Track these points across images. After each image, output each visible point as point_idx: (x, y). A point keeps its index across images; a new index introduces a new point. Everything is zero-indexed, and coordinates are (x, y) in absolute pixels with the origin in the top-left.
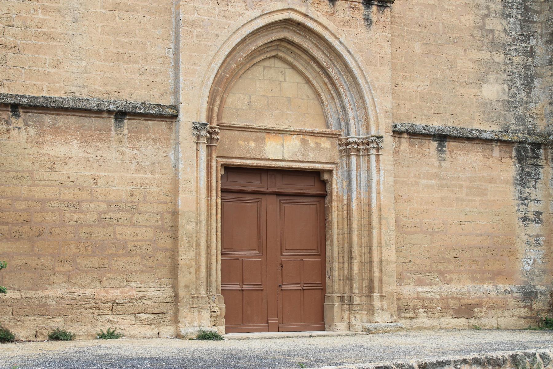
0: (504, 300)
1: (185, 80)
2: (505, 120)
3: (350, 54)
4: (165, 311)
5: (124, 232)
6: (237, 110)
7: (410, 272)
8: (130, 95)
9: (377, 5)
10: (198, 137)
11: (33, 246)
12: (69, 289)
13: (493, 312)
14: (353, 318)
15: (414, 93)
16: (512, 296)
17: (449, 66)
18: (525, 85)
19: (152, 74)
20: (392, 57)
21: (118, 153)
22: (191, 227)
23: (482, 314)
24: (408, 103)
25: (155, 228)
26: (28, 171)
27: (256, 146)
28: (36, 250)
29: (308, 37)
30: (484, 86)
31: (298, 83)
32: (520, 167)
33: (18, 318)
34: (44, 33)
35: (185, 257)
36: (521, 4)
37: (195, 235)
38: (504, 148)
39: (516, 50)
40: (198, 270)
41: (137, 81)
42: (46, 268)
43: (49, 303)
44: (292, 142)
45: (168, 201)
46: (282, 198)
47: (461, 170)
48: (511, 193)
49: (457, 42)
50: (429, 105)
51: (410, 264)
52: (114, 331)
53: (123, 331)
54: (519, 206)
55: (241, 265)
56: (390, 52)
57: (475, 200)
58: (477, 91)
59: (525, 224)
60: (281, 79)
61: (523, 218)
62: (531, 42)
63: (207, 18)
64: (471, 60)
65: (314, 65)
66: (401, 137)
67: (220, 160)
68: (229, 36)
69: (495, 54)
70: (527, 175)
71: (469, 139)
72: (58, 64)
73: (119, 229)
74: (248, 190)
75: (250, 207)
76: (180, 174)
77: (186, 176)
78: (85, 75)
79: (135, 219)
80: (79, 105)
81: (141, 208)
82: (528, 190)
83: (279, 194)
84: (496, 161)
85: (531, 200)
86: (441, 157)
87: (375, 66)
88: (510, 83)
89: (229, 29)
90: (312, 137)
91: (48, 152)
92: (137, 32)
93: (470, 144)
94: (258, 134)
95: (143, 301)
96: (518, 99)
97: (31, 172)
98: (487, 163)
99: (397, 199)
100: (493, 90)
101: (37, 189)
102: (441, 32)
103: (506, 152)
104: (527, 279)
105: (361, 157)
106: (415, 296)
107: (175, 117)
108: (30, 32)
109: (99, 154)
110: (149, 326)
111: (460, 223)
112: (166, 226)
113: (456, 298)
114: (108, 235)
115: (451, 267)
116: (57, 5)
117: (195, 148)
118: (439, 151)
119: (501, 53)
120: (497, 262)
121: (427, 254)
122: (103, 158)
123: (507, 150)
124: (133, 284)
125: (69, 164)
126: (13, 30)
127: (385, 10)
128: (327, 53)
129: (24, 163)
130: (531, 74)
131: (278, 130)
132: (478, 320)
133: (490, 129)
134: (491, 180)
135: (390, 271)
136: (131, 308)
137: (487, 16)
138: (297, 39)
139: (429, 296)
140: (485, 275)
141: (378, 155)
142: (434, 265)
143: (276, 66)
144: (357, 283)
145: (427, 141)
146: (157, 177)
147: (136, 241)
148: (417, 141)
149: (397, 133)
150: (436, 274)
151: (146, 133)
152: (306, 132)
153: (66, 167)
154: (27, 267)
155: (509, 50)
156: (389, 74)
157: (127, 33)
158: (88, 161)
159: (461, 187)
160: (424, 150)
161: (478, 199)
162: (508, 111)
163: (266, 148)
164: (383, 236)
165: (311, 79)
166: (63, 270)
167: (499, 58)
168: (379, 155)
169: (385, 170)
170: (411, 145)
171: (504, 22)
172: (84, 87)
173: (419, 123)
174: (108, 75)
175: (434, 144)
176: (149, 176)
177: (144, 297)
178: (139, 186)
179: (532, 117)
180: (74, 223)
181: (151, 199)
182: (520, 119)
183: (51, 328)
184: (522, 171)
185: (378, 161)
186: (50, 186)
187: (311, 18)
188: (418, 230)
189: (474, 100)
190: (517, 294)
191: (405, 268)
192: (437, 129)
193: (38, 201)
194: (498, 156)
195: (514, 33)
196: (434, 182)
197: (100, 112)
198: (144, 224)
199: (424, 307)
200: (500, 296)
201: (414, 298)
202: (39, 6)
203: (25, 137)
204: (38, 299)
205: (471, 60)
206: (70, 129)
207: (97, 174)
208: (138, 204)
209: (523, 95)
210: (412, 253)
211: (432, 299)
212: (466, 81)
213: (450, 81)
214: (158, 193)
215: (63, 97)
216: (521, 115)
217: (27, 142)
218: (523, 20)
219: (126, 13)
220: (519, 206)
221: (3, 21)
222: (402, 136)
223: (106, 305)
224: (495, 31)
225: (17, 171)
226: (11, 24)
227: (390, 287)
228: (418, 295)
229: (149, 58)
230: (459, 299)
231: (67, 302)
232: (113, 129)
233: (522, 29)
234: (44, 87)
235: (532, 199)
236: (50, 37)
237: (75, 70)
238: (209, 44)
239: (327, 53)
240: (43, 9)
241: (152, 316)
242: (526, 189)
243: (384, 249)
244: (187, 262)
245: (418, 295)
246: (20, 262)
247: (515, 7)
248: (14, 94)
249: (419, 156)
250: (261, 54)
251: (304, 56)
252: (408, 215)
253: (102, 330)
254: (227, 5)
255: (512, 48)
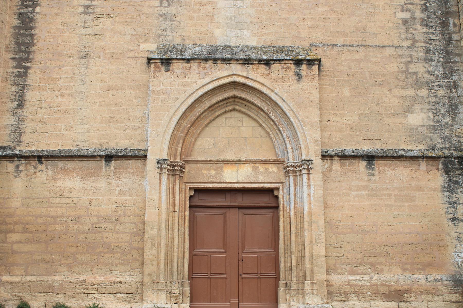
0: (433, 287)
1: (152, 131)
2: (431, 140)
3: (284, 101)
4: (136, 292)
5: (109, 237)
6: (205, 149)
7: (343, 264)
8: (117, 144)
9: (306, 64)
10: (161, 169)
11: (47, 247)
12: (70, 275)
13: (423, 297)
14: (292, 301)
15: (344, 126)
16: (442, 283)
17: (376, 103)
18: (449, 112)
19: (133, 129)
20: (320, 101)
21: (107, 183)
22: (154, 232)
23: (412, 299)
24: (339, 134)
25: (132, 233)
26: (47, 198)
27: (216, 174)
28: (50, 249)
29: (252, 93)
30: (410, 115)
31: (253, 127)
32: (448, 177)
33: (33, 294)
34: (61, 110)
35: (150, 253)
36: (443, 50)
37: (156, 238)
38: (431, 163)
39: (439, 85)
40: (158, 263)
41: (122, 135)
42: (55, 261)
43: (54, 285)
44: (245, 169)
45: (141, 215)
46: (244, 210)
47: (390, 182)
48: (439, 200)
49: (383, 84)
50: (358, 133)
51: (343, 257)
52: (98, 305)
53: (105, 305)
54: (447, 208)
55: (209, 259)
56: (318, 96)
57: (404, 206)
58: (402, 120)
59: (454, 224)
60: (240, 125)
61: (453, 218)
62: (453, 78)
63: (170, 87)
64: (397, 97)
65: (262, 113)
66: (333, 160)
67: (187, 185)
68: (185, 98)
69: (419, 90)
70: (455, 183)
71: (394, 157)
72: (69, 128)
73: (105, 235)
74: (260, 206)
75: (217, 218)
76: (147, 195)
77: (151, 196)
78: (87, 134)
79: (117, 227)
80: (80, 153)
81: (122, 220)
82: (457, 196)
83: (240, 208)
84: (423, 173)
85: (460, 204)
86: (370, 173)
87: (305, 108)
88: (435, 112)
89: (186, 93)
90: (262, 164)
91: (60, 185)
92: (123, 103)
93: (397, 162)
94: (218, 165)
95: (120, 284)
96: (443, 123)
97: (49, 198)
98: (415, 175)
99: (326, 206)
100: (418, 118)
101: (52, 209)
102: (368, 78)
103: (432, 165)
104: (458, 269)
105: (298, 176)
106: (346, 283)
107: (146, 156)
108: (52, 110)
109: (93, 184)
110: (123, 303)
111: (390, 224)
112: (139, 232)
113: (386, 285)
114: (98, 239)
115: (382, 260)
116: (71, 92)
117: (158, 177)
118: (368, 168)
119: (425, 89)
120: (427, 255)
121: (358, 249)
122: (96, 187)
123: (434, 164)
124: (115, 273)
125: (73, 192)
126: (42, 110)
127: (314, 67)
128: (268, 103)
129: (44, 193)
130: (455, 103)
131: (233, 161)
132: (408, 303)
133: (417, 149)
134: (419, 189)
135: (320, 263)
136: (111, 289)
137: (409, 62)
138: (243, 95)
139: (359, 283)
140: (415, 267)
141: (309, 174)
142: (365, 259)
143: (235, 116)
144: (295, 273)
145: (357, 162)
146: (134, 198)
147: (117, 243)
148: (347, 162)
149: (324, 156)
150: (368, 266)
151: (126, 169)
152: (255, 161)
153: (71, 194)
154: (43, 260)
155: (433, 86)
156: (318, 113)
157: (116, 104)
158: (86, 189)
159: (390, 195)
160: (355, 168)
161: (406, 204)
162: (434, 133)
163: (224, 174)
164: (314, 236)
165: (261, 123)
166: (66, 262)
167: (424, 93)
168: (310, 174)
169: (315, 185)
170: (342, 165)
171: (426, 65)
172: (85, 142)
173: (349, 149)
174: (102, 133)
175: (363, 164)
176: (128, 198)
177: (120, 282)
178: (121, 205)
179: (459, 137)
180: (75, 231)
181: (129, 213)
182: (444, 139)
183: (55, 301)
184: (450, 180)
185: (309, 179)
186: (60, 207)
187: (252, 79)
188: (349, 230)
189: (401, 127)
190: (447, 282)
191: (339, 261)
192: (365, 152)
193: (51, 217)
194: (425, 169)
195: (436, 72)
196: (364, 192)
197: (93, 157)
198: (123, 231)
199: (354, 292)
200: (430, 284)
201: (345, 285)
202: (59, 94)
203: (46, 176)
204: (47, 282)
205: (397, 97)
206: (75, 169)
207: (92, 198)
208: (120, 217)
209: (448, 119)
210: (344, 249)
211: (363, 286)
212: (392, 113)
213: (377, 114)
214: (134, 209)
215: (72, 149)
216: (447, 136)
217: (46, 179)
218: (445, 62)
219: (116, 91)
220: (447, 208)
221: (37, 106)
222: (334, 159)
223: (94, 287)
224: (419, 73)
225: (39, 198)
226: (41, 107)
227: (321, 276)
228: (349, 282)
229: (131, 119)
230: (389, 286)
231: (67, 284)
232: (104, 167)
233: (444, 68)
234: (60, 143)
235: (461, 202)
236: (65, 112)
237: (80, 131)
238: (171, 105)
239: (268, 103)
240: (62, 95)
241: (126, 295)
242: (455, 194)
243: (315, 246)
244: (150, 257)
245: (349, 282)
246: (38, 257)
247: (436, 53)
248: (40, 149)
249: (350, 173)
250: (221, 109)
251: (253, 107)
252: (340, 219)
253: (89, 304)
254: (185, 77)
255: (435, 84)
